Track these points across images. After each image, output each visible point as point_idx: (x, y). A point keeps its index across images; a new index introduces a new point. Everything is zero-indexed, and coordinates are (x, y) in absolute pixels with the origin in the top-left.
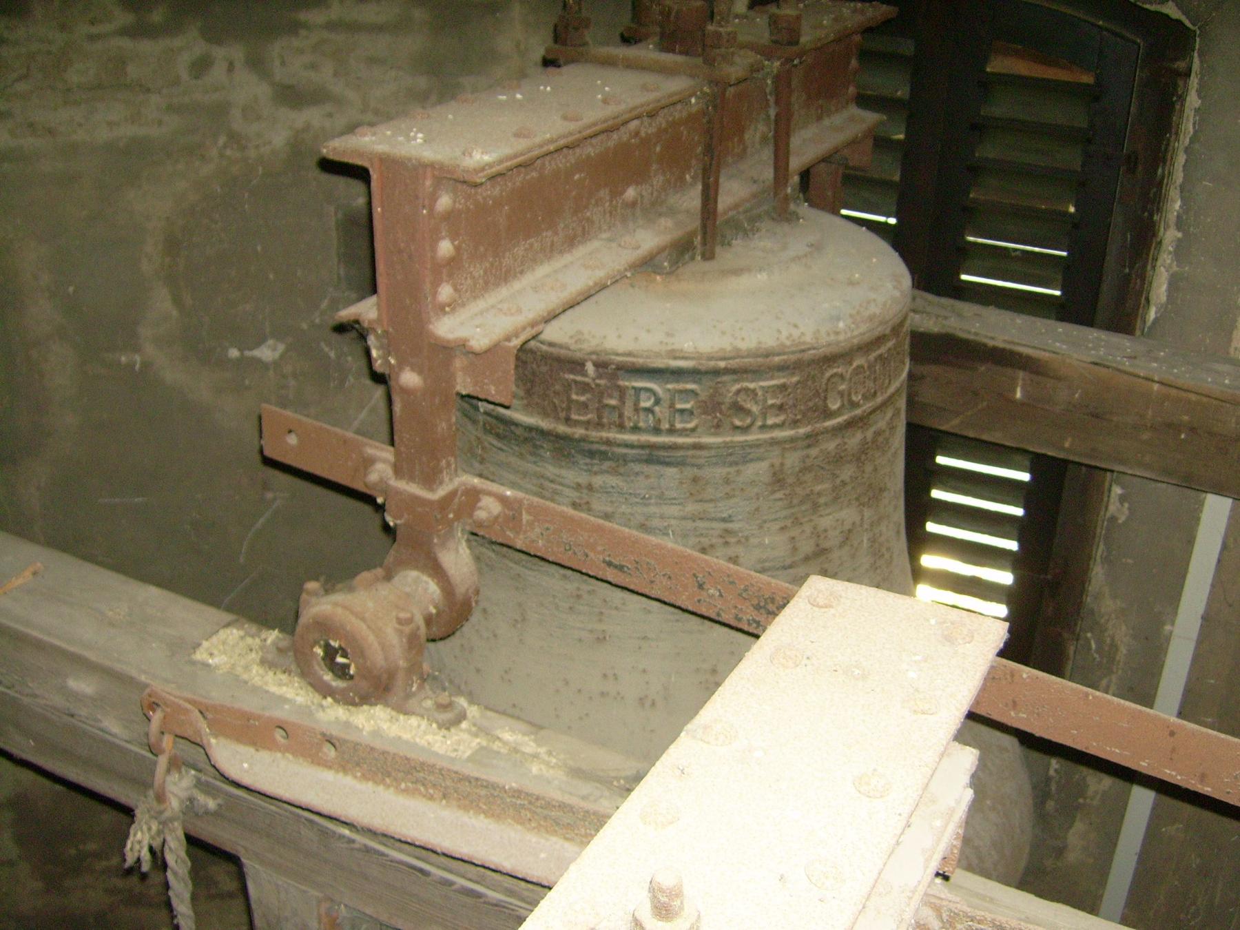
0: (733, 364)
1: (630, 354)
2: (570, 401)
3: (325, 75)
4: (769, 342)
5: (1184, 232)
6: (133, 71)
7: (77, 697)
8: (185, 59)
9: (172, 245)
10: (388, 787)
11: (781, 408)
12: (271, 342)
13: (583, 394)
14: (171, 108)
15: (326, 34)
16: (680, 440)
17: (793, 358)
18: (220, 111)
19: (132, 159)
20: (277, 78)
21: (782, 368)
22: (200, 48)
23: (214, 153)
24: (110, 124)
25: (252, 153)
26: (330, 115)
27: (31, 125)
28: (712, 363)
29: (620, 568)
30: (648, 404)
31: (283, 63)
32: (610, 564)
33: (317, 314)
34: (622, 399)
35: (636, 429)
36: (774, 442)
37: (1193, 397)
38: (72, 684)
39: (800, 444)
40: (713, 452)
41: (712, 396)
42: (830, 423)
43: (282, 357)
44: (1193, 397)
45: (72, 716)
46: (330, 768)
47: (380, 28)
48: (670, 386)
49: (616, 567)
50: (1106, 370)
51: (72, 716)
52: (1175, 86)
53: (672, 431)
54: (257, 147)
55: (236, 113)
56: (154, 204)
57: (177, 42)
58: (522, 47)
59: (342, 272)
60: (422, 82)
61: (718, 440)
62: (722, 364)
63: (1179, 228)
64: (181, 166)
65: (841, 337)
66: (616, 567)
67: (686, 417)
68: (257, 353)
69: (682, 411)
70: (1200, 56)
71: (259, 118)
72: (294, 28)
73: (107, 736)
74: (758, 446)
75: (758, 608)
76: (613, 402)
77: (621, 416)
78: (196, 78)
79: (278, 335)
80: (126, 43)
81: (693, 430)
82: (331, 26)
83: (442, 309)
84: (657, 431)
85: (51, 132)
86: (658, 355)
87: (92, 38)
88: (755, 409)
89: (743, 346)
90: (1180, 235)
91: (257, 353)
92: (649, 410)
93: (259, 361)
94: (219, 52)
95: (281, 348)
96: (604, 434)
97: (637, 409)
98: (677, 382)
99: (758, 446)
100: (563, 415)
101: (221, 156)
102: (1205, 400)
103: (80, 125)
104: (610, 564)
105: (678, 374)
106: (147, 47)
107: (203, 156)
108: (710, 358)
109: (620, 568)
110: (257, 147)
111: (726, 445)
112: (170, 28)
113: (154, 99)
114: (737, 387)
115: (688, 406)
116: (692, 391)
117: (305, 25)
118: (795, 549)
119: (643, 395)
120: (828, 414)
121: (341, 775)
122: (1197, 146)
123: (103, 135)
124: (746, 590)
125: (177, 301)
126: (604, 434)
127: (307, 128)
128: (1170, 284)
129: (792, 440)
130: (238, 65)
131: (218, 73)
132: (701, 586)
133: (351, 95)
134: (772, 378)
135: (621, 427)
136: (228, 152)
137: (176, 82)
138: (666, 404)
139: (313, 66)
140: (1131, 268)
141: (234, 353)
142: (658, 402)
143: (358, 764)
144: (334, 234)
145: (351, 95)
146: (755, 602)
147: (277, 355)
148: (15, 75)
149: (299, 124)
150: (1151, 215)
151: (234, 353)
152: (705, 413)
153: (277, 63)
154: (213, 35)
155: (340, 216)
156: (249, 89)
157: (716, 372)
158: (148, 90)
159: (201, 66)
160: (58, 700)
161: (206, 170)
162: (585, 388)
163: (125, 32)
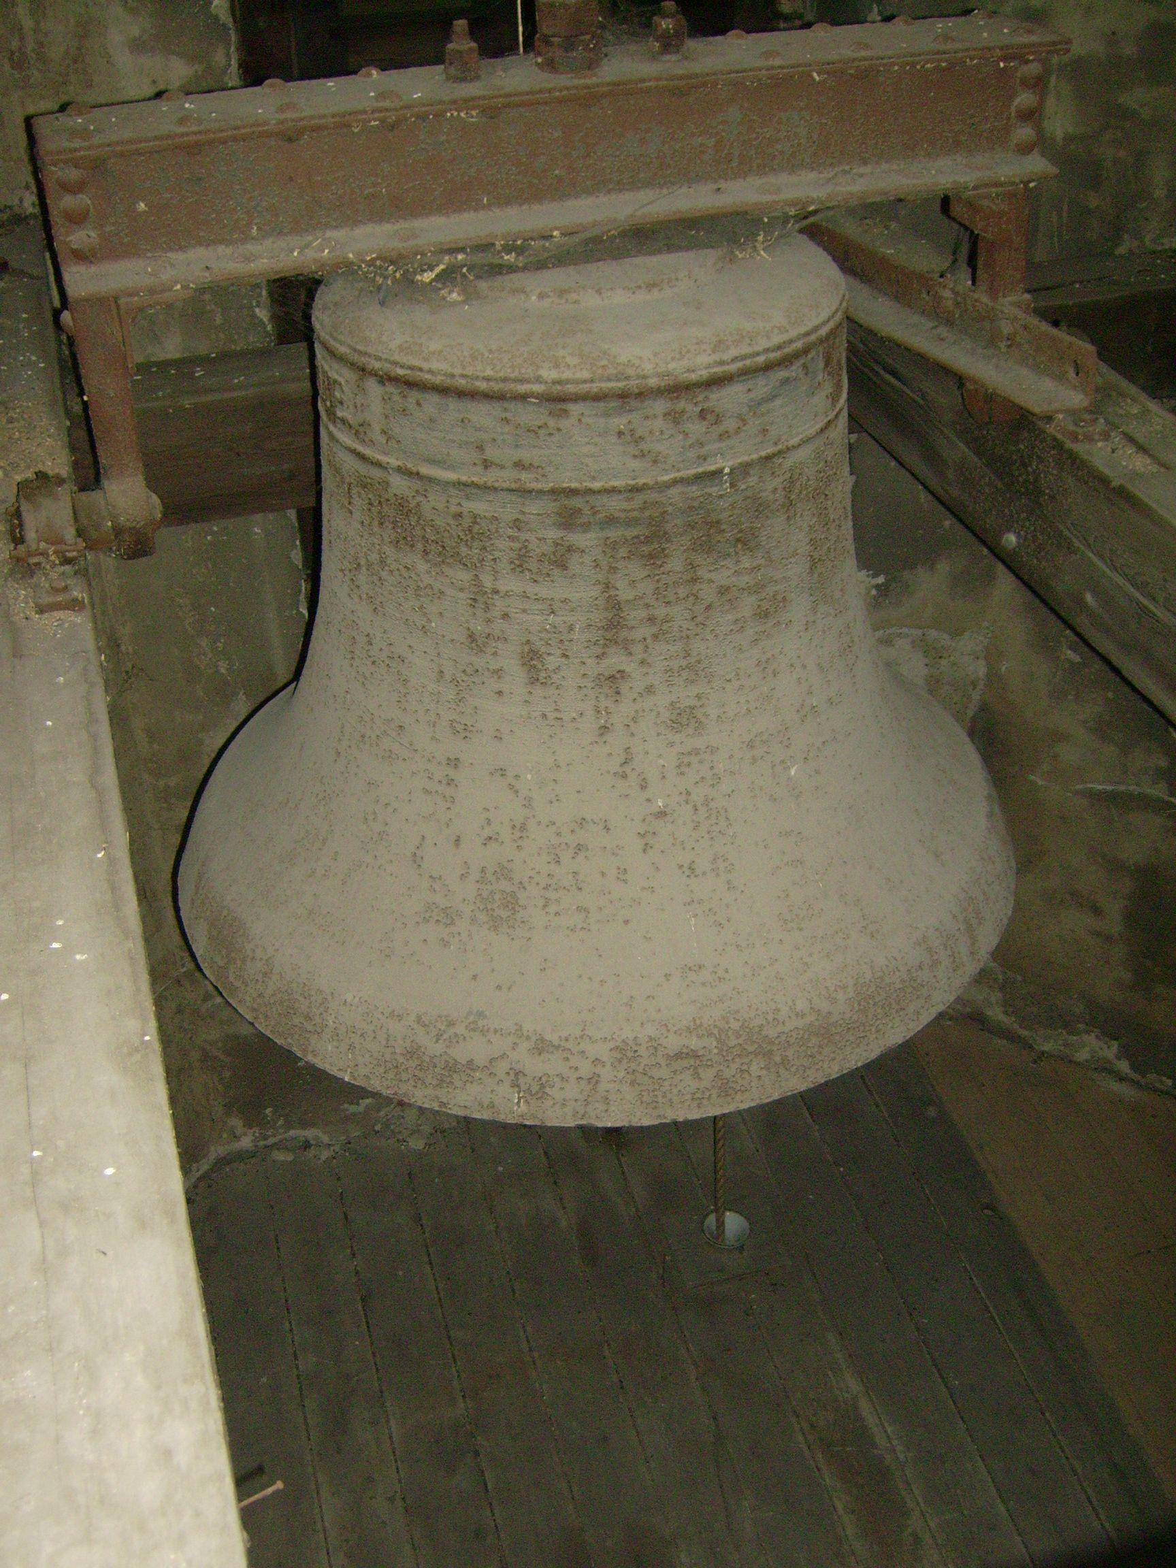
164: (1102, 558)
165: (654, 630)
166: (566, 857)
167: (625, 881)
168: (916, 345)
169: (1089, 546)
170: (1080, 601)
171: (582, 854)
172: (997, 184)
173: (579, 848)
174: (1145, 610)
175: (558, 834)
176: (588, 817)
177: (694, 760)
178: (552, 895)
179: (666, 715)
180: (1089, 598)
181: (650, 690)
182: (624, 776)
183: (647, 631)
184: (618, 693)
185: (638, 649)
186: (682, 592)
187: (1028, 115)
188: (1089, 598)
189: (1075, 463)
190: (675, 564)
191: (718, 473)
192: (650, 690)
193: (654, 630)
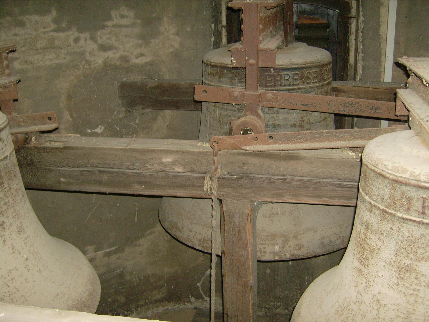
0: (306, 66)
1: (282, 65)
2: (267, 81)
3: (113, 41)
4: (313, 60)
5: (364, 54)
6: (57, 43)
7: (166, 164)
8: (72, 38)
9: (69, 97)
10: (289, 144)
11: (316, 77)
12: (100, 126)
13: (270, 78)
14: (68, 53)
15: (113, 29)
16: (296, 87)
17: (318, 64)
18: (83, 54)
19: (57, 71)
20: (99, 43)
21: (316, 67)
22: (76, 34)
23: (81, 67)
24: (50, 60)
25: (92, 66)
26: (115, 53)
27: (26, 61)
28: (302, 66)
29: (306, 105)
30: (287, 78)
31: (101, 38)
32: (303, 105)
33: (113, 116)
34: (281, 77)
35: (285, 85)
36: (316, 87)
37: (381, 90)
38: (164, 160)
39: (320, 88)
40: (303, 90)
41: (302, 75)
42: (326, 82)
43: (104, 131)
44: (381, 90)
45: (163, 171)
46: (271, 144)
47: (127, 26)
48: (292, 73)
49: (305, 105)
50: (357, 87)
51: (163, 171)
52: (349, 22)
53: (293, 85)
54: (94, 64)
55: (87, 54)
56: (64, 85)
57: (70, 33)
58: (167, 30)
59: (120, 102)
60: (140, 42)
61: (304, 86)
62: (304, 66)
63: (362, 53)
64: (72, 72)
65: (326, 60)
66: (305, 105)
67: (296, 81)
68: (96, 130)
69: (295, 79)
70: (362, 7)
71: (94, 55)
72: (103, 27)
73: (176, 174)
74: (312, 88)
75: (344, 106)
76: (278, 79)
77: (281, 82)
78: (76, 44)
79: (102, 124)
80: (55, 34)
81: (298, 84)
82: (114, 26)
83: (261, 42)
84: (290, 85)
85: (32, 63)
86: (289, 64)
87: (44, 33)
88: (311, 78)
89: (308, 61)
90: (363, 55)
91: (96, 130)
92: (288, 80)
93: (97, 133)
94: (82, 35)
95: (103, 128)
96: (276, 88)
97: (285, 80)
98: (294, 71)
99: (312, 88)
100: (264, 85)
101: (84, 68)
102: (384, 90)
103: (41, 60)
104: (303, 105)
105: (294, 69)
106: (61, 35)
107: (78, 68)
108: (301, 65)
109: (306, 105)
110: (94, 64)
111: (306, 88)
112: (68, 28)
113: (63, 51)
114: (307, 72)
115: (297, 78)
116: (298, 73)
117: (107, 26)
118: (321, 117)
119: (286, 76)
120: (325, 80)
121: (274, 145)
122: (364, 30)
123: (48, 63)
124: (341, 102)
125: (72, 116)
126: (276, 88)
127: (108, 58)
128: (362, 68)
129: (319, 86)
130: (88, 39)
131: (82, 42)
132: (329, 104)
133: (121, 47)
134: (314, 69)
135: (281, 85)
136: (86, 67)
137: (70, 45)
138: (291, 77)
139: (109, 39)
140: (343, 72)
141: (89, 131)
142: (289, 77)
143: (280, 140)
144: (117, 90)
145: (121, 47)
146: (344, 105)
147: (102, 130)
148: (21, 46)
149: (106, 57)
150: (347, 58)
151: (89, 131)
152: (301, 79)
153: (99, 38)
154: (81, 30)
155: (119, 84)
156: (91, 46)
157: (303, 68)
158: (61, 48)
159: (77, 40)
160: (158, 168)
161: (80, 72)
162: (271, 76)
163: (54, 31)
164: (64, 167)
165: (7, 206)
166: (10, 284)
167: (28, 282)
168: (218, 62)
169: (58, 166)
170: (60, 182)
171: (14, 281)
172: (12, 82)
173: (13, 279)
174: (81, 171)
175: (5, 278)
176: (11, 270)
177: (27, 241)
178: (12, 297)
179: (17, 230)
180: (62, 179)
181: (11, 225)
182: (15, 252)
183: (5, 207)
184: (4, 228)
185: (5, 213)
186: (9, 193)
187: (7, 67)
188: (62, 179)
189: (45, 149)
190: (6, 185)
191: (7, 156)
192: (11, 225)
193: (7, 206)
